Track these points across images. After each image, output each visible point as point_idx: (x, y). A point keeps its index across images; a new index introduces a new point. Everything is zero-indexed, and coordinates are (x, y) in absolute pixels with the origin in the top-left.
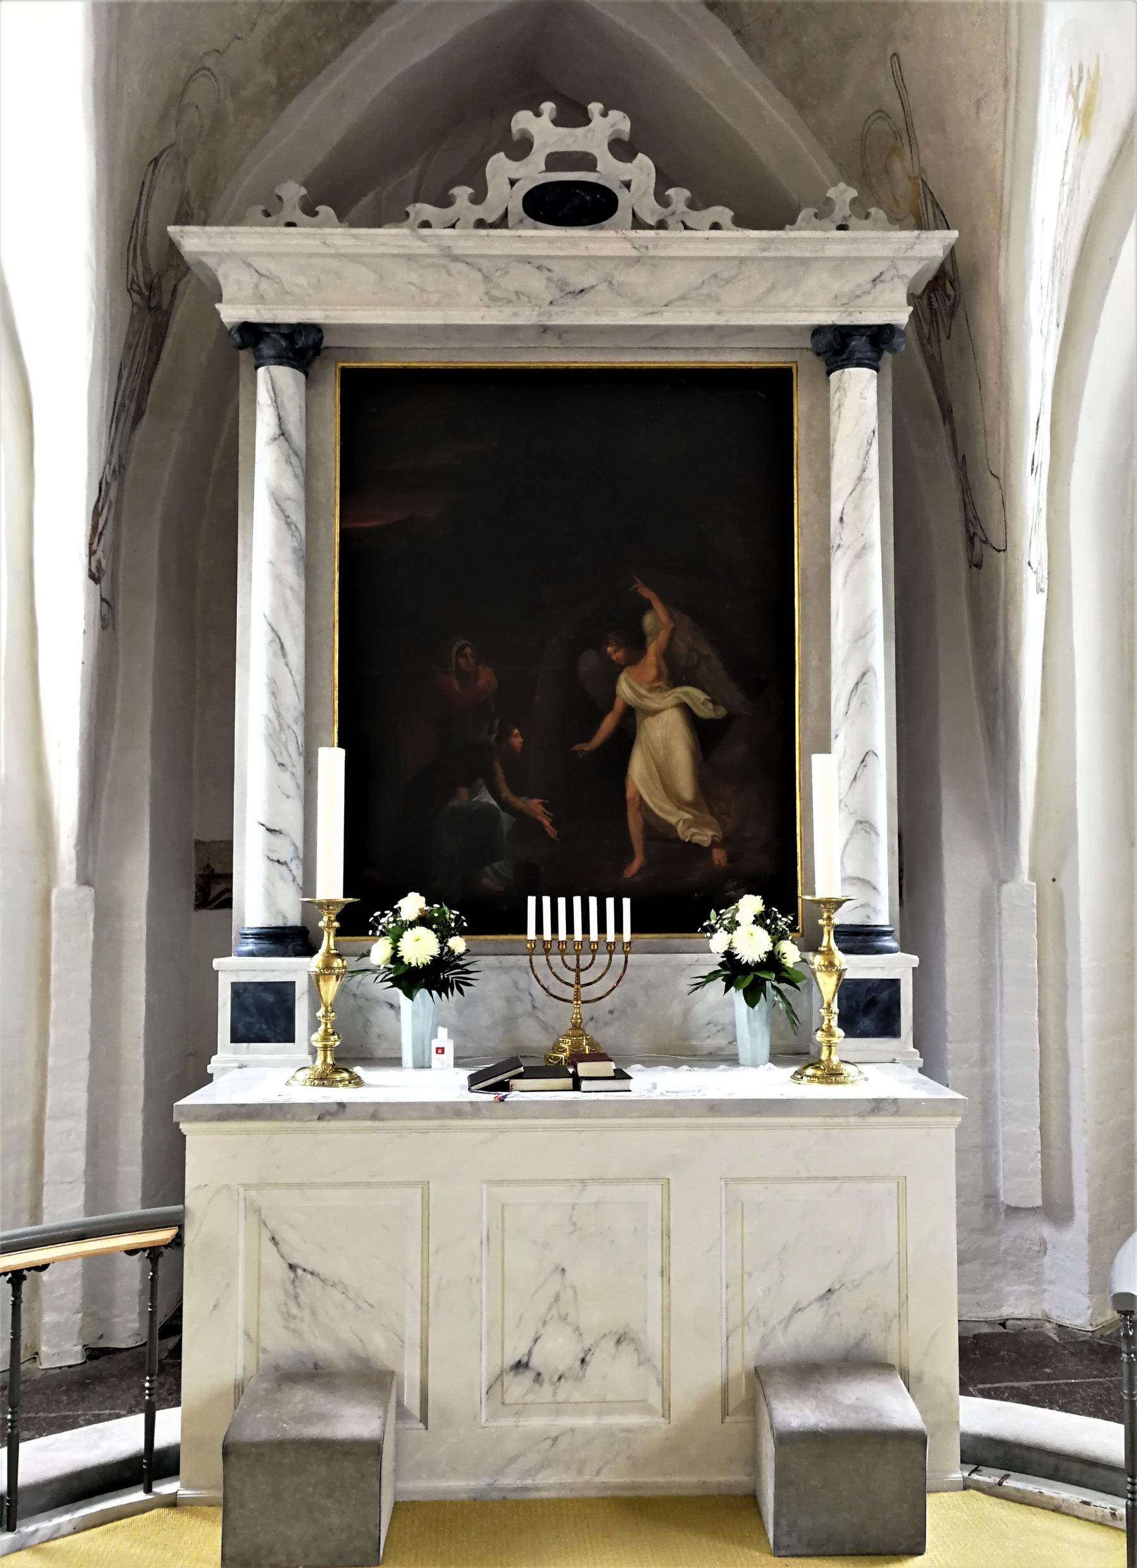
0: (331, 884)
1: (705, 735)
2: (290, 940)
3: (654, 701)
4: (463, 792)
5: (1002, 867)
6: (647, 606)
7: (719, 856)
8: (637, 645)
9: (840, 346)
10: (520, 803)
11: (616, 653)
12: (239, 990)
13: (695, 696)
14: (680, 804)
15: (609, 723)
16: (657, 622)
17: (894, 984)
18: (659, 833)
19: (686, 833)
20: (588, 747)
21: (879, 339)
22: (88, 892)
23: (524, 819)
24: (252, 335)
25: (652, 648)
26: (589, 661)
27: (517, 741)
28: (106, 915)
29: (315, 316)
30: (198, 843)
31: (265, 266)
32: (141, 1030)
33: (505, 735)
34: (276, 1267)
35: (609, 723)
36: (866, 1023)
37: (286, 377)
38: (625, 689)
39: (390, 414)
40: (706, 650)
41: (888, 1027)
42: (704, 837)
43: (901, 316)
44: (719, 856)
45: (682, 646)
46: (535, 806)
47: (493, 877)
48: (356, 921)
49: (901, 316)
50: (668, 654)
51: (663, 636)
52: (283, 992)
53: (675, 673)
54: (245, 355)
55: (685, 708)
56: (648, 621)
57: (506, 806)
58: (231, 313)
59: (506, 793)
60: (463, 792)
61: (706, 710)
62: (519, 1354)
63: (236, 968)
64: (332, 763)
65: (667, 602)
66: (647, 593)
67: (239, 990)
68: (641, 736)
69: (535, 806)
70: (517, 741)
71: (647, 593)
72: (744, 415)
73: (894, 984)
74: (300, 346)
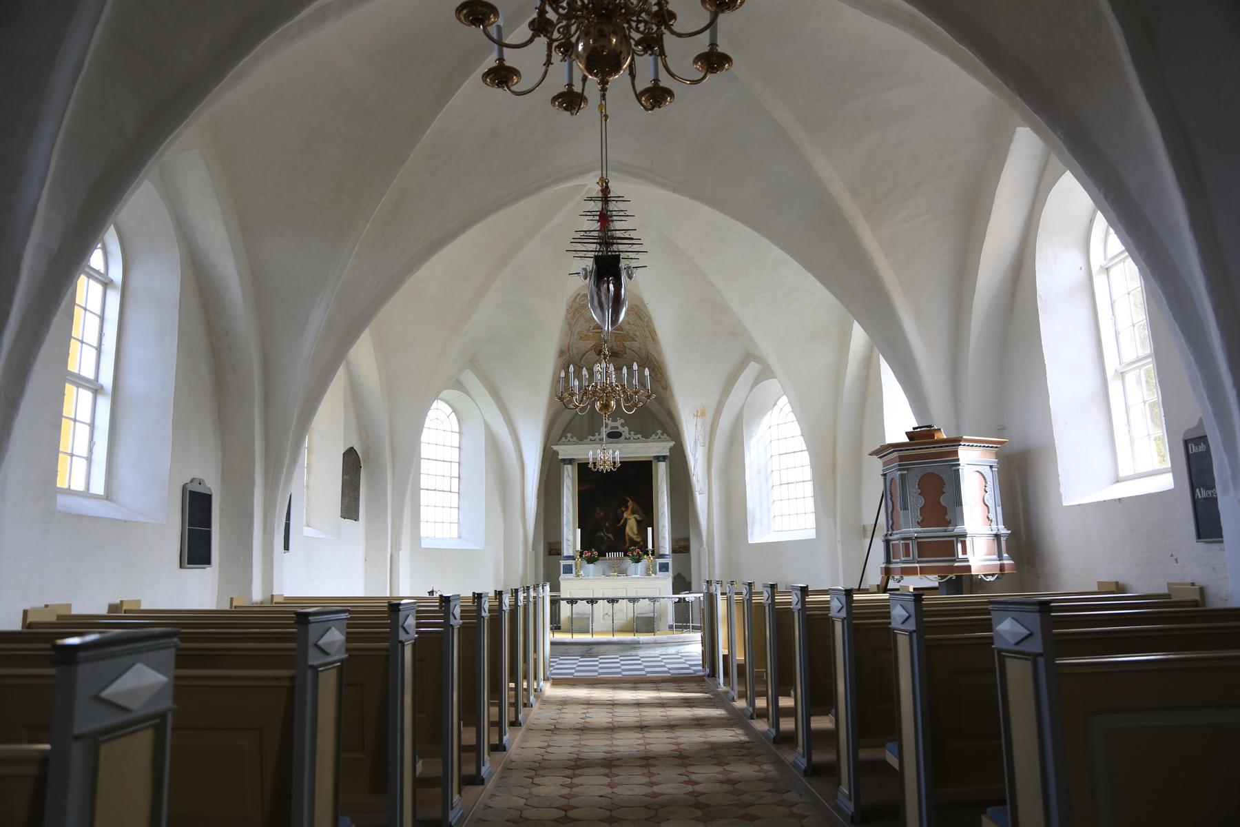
0: (579, 547)
1: (639, 523)
2: (573, 558)
5: (702, 545)
8: (627, 507)
16: (630, 504)
21: (664, 458)
28: (536, 556)
31: (565, 451)
41: (667, 570)
53: (633, 512)
74: (570, 461)
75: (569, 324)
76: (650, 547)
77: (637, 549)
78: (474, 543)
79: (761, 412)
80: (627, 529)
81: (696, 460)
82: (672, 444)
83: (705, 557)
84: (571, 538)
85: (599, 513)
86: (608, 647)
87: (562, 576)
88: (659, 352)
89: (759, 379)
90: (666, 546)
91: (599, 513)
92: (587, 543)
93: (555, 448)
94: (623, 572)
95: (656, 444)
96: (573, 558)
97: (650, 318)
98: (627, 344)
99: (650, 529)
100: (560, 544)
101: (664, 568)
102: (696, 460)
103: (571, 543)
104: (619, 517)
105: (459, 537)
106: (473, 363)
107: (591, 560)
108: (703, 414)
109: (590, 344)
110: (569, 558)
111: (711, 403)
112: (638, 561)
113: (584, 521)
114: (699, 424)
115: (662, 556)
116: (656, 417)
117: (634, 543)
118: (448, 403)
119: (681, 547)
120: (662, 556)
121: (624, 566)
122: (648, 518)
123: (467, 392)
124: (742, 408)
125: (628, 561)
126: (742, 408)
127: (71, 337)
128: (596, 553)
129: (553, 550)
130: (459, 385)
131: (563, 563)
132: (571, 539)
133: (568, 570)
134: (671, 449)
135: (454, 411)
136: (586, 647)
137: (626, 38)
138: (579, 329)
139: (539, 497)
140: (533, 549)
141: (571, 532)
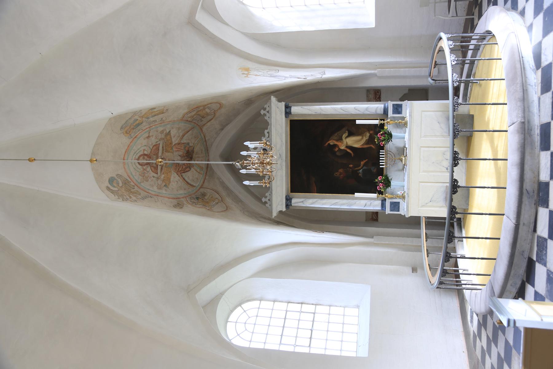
0: (374, 195)
1: (351, 134)
2: (384, 201)
3: (345, 143)
4: (360, 175)
5: (374, 75)
6: (329, 144)
7: (371, 132)
8: (335, 146)
9: (288, 113)
10: (362, 166)
11: (337, 149)
12: (391, 210)
13: (344, 136)
14: (362, 138)
15: (349, 151)
16: (332, 142)
17: (393, 105)
18: (367, 142)
19: (367, 138)
20: (352, 154)
21: (287, 107)
22: (374, 237)
23: (364, 165)
24: (288, 205)
25: (336, 143)
26: (338, 154)
27: (351, 166)
28: (378, 234)
29: (284, 196)
30: (366, 220)
31: (278, 204)
32: (399, 229)
33: (350, 168)
34: (430, 204)
35: (349, 151)
36: (400, 110)
37: (293, 201)
38: (343, 148)
39: (299, 184)
40: (336, 134)
41: (401, 106)
42: (368, 135)
43: (283, 103)
44: (371, 132)
45: (336, 138)
46: (362, 163)
47: (374, 170)
48: (380, 193)
49: (283, 103)
50: (337, 140)
51: (334, 141)
52: (392, 203)
53: (340, 139)
54: (290, 207)
55: (346, 138)
56: (331, 144)
57: (362, 168)
58: (284, 209)
59: (360, 168)
60: (360, 175)
61: (347, 134)
62: (445, 169)
63: (388, 211)
64: (357, 195)
65: (328, 141)
66: (327, 144)
67: (391, 210)
68: (351, 145)
69: (362, 163)
70: (351, 166)
71: (327, 144)
72: (300, 130)
73: (393, 105)
74: (288, 200)
75: (144, 198)
76: (376, 122)
77: (377, 134)
78: (363, 294)
79: (250, 17)
80: (356, 146)
81: (291, 77)
82: (273, 99)
83: (387, 72)
84: (363, 202)
85: (340, 173)
86: (527, 167)
87: (402, 212)
88: (177, 107)
89: (214, 14)
90: (376, 107)
91: (340, 173)
92: (369, 186)
93: (275, 214)
94: (402, 151)
95: (273, 115)
96: (384, 201)
97: (135, 113)
98: (175, 141)
99: (358, 122)
100: (367, 213)
101: (398, 109)
102: (291, 77)
103: (368, 202)
104: (345, 154)
105: (358, 307)
106: (190, 290)
107: (387, 183)
108: (248, 70)
109: (175, 177)
110: (383, 205)
111: (237, 62)
112: (390, 135)
113: (348, 189)
114: (256, 73)
115: (386, 111)
116: (249, 114)
117: (371, 140)
118: (232, 311)
119: (375, 95)
120: (386, 111)
121: (394, 150)
122: (347, 125)
123: (222, 294)
124: (242, 33)
125: (391, 146)
126: (242, 33)
127: (264, 349)
128: (380, 178)
129: (373, 218)
130: (214, 302)
131: (388, 211)
132: (364, 202)
133: (395, 206)
134: (280, 101)
135: (240, 305)
136: (525, 198)
137: (340, 175)
138: (155, 188)
139: (323, 231)
140: (372, 237)
141: (358, 202)
